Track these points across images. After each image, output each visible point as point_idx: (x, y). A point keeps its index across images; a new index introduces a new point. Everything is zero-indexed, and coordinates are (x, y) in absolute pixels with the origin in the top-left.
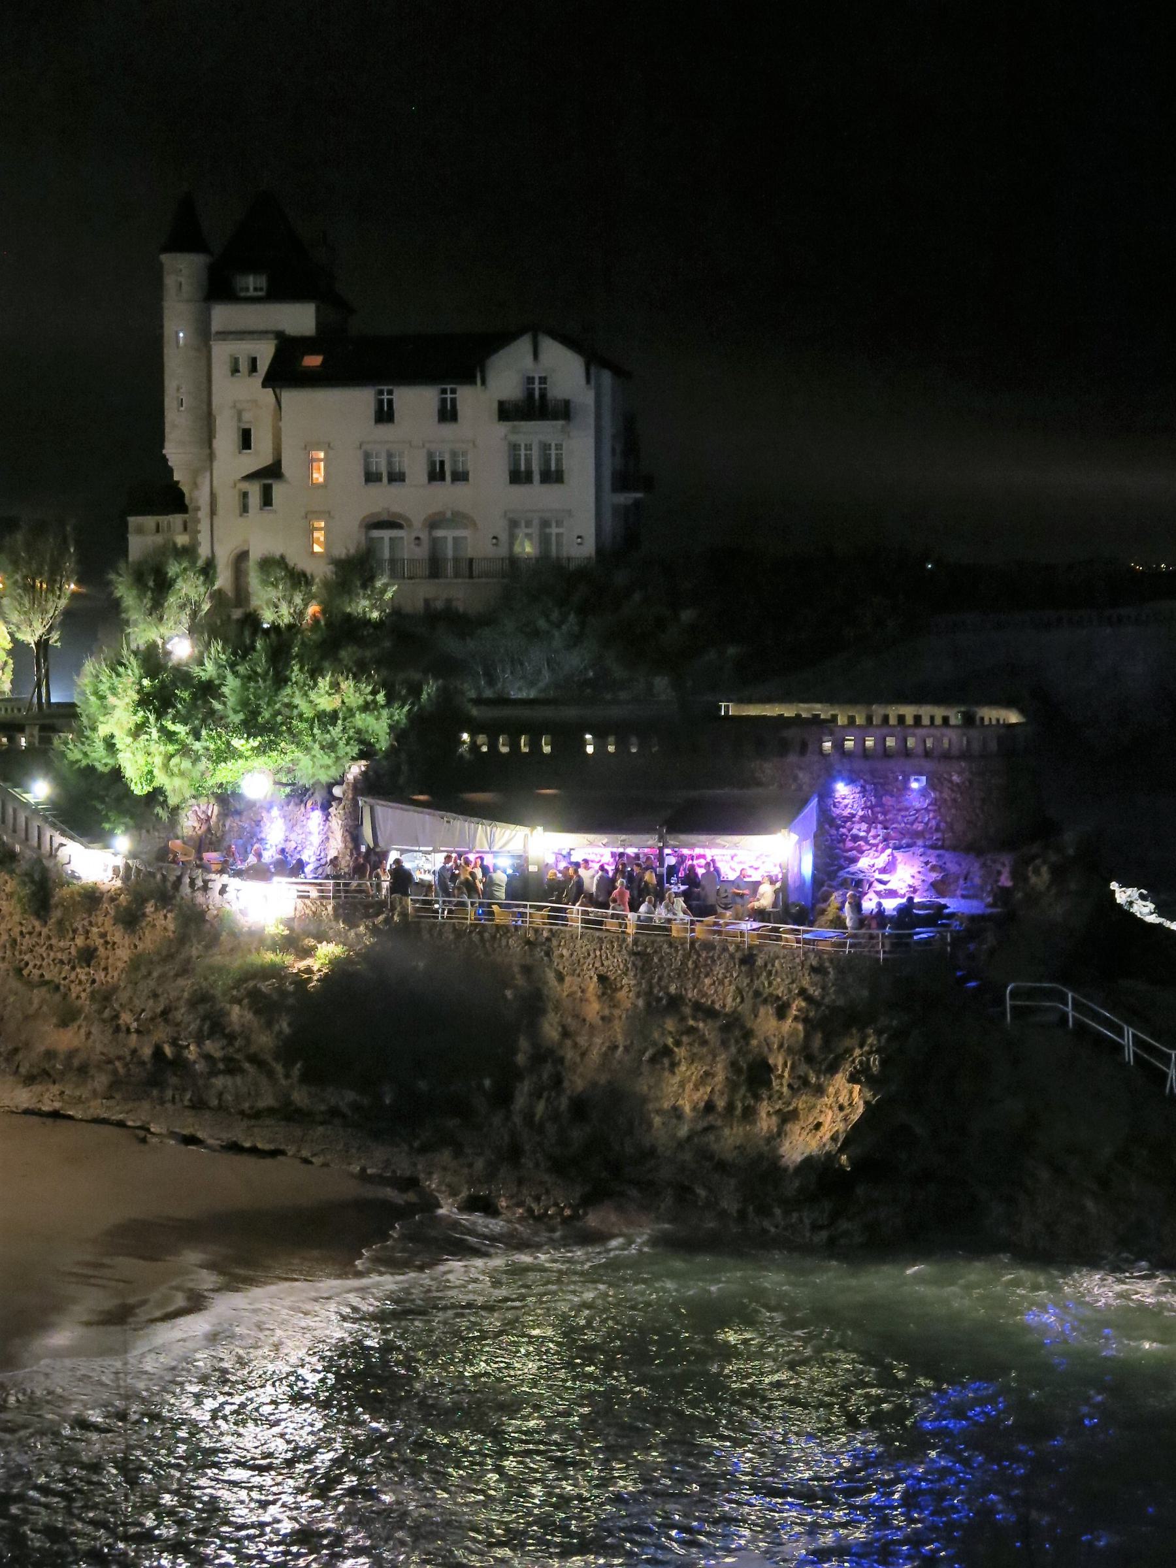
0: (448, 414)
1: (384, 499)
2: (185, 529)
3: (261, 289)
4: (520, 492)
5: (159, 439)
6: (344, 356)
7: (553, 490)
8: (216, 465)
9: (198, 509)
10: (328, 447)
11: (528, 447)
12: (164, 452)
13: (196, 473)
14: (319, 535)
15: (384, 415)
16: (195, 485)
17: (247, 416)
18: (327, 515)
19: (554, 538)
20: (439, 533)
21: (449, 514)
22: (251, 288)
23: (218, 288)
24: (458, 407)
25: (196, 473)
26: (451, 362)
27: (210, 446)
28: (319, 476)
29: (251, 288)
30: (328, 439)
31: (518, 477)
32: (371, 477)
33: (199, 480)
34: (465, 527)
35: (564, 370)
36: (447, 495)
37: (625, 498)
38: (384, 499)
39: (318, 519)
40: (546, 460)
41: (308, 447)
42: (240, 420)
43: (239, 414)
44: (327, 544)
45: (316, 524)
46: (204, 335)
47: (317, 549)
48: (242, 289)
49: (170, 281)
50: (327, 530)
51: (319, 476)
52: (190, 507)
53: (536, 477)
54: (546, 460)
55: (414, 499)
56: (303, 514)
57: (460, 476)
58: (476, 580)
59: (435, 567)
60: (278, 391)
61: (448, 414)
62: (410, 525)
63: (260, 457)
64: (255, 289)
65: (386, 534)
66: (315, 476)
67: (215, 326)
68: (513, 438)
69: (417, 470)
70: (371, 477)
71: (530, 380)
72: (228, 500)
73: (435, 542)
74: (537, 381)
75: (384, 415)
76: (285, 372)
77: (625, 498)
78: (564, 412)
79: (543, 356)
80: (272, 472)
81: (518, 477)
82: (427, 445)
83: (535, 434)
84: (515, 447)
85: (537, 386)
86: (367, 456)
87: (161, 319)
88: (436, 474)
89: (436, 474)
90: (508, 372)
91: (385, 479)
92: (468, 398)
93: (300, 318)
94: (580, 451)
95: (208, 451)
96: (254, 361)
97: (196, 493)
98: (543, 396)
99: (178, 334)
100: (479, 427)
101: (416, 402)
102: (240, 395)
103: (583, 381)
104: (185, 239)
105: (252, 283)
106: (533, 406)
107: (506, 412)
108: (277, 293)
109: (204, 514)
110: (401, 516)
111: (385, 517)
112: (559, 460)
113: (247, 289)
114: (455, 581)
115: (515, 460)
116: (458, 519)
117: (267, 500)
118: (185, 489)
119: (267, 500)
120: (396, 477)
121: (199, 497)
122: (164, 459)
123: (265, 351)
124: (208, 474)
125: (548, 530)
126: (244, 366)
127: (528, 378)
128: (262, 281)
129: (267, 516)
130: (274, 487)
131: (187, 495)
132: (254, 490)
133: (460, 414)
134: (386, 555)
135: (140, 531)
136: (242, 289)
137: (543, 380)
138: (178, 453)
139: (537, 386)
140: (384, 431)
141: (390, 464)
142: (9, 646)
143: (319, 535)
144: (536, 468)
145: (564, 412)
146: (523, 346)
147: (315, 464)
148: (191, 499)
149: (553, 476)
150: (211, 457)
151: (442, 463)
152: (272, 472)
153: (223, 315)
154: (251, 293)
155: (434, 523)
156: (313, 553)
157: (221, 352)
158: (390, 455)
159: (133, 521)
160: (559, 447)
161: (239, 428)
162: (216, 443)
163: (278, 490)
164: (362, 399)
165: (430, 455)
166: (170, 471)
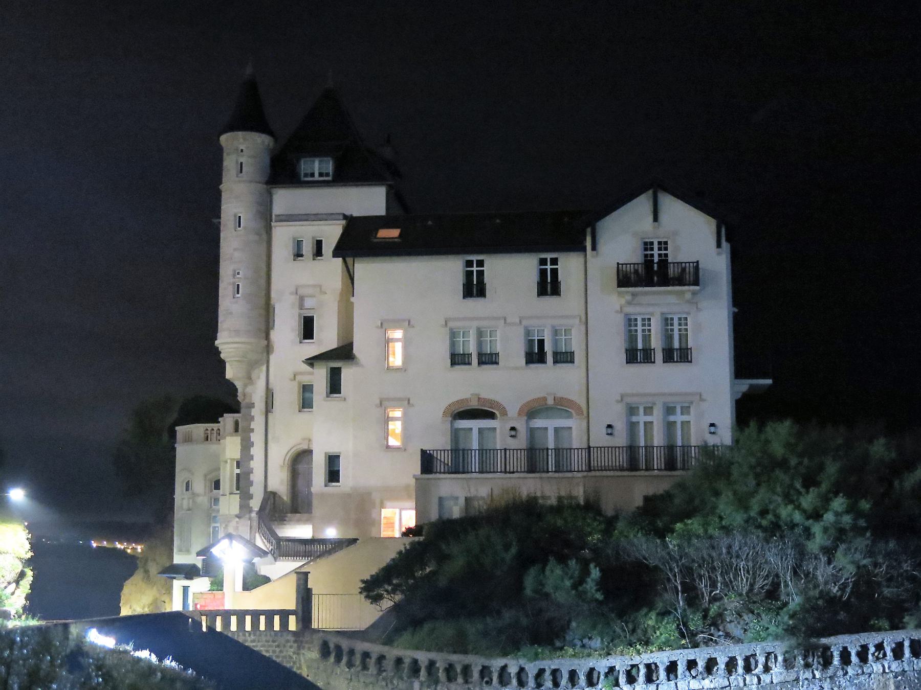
0: (549, 285)
1: (473, 384)
2: (236, 430)
3: (327, 175)
4: (640, 370)
5: (211, 328)
6: (422, 226)
7: (677, 370)
8: (273, 358)
9: (252, 406)
10: (407, 324)
11: (647, 321)
12: (216, 342)
13: (252, 366)
14: (396, 427)
15: (474, 288)
16: (249, 379)
17: (308, 303)
18: (406, 403)
19: (679, 426)
20: (538, 423)
21: (550, 402)
22: (317, 174)
23: (281, 172)
24: (560, 278)
25: (252, 366)
26: (558, 228)
27: (267, 337)
28: (396, 359)
29: (317, 174)
30: (407, 314)
31: (636, 355)
32: (458, 359)
33: (254, 375)
34: (569, 416)
35: (691, 233)
36: (548, 379)
37: (744, 385)
38: (473, 384)
39: (395, 407)
40: (669, 337)
41: (384, 325)
42: (301, 307)
43: (302, 299)
44: (406, 435)
45: (391, 414)
46: (266, 218)
47: (393, 442)
48: (306, 175)
49: (229, 163)
50: (405, 420)
51: (396, 359)
52: (243, 404)
53: (659, 356)
54: (669, 337)
55: (510, 384)
56: (378, 402)
57: (564, 357)
58: (593, 473)
59: (534, 460)
60: (349, 260)
61: (549, 285)
62: (504, 413)
63: (327, 338)
64: (321, 175)
65: (475, 424)
66: (391, 359)
67: (277, 209)
68: (629, 309)
69: (512, 350)
70: (458, 359)
71: (648, 246)
72: (286, 396)
73: (532, 432)
74: (656, 246)
75: (474, 288)
76: (358, 241)
77: (744, 385)
78: (690, 276)
79: (663, 217)
80: (344, 352)
81: (636, 355)
82: (525, 323)
83: (657, 303)
84: (630, 322)
85: (656, 252)
86: (453, 335)
87: (220, 201)
88: (535, 355)
89: (535, 355)
90: (623, 235)
91: (475, 360)
92: (569, 266)
93: (370, 201)
94: (711, 323)
95: (266, 342)
96: (319, 244)
97: (249, 389)
98: (664, 262)
99: (237, 200)
100: (591, 291)
101: (510, 272)
102: (307, 281)
103: (713, 242)
104: (250, 119)
105: (318, 166)
106: (653, 271)
107: (625, 279)
108: (345, 175)
109: (258, 412)
110: (492, 403)
111: (474, 405)
112: (683, 337)
113: (312, 175)
114: (557, 475)
115: (631, 338)
116: (561, 407)
117: (334, 387)
118: (239, 385)
119: (334, 387)
120: (488, 359)
121: (253, 394)
122: (217, 352)
123: (332, 233)
124: (264, 368)
125: (672, 418)
126: (308, 249)
127: (645, 243)
128: (329, 166)
129: (334, 403)
130: (343, 370)
131: (239, 390)
132: (319, 377)
133: (563, 288)
134: (475, 445)
135: (188, 439)
136: (306, 175)
137: (663, 245)
138: (231, 342)
139: (656, 252)
140: (475, 305)
141: (480, 344)
142: (410, 630)
143: (396, 427)
144: (656, 343)
145: (690, 276)
146: (641, 205)
147: (391, 344)
148: (244, 395)
149: (678, 354)
150: (268, 349)
151: (541, 343)
152: (344, 352)
153: (284, 199)
154: (317, 177)
155: (533, 411)
156: (388, 447)
157: (283, 235)
158: (480, 334)
159: (181, 430)
160: (683, 321)
161: (300, 315)
162: (274, 335)
163: (348, 374)
164: (448, 270)
165: (528, 333)
166: (222, 364)
